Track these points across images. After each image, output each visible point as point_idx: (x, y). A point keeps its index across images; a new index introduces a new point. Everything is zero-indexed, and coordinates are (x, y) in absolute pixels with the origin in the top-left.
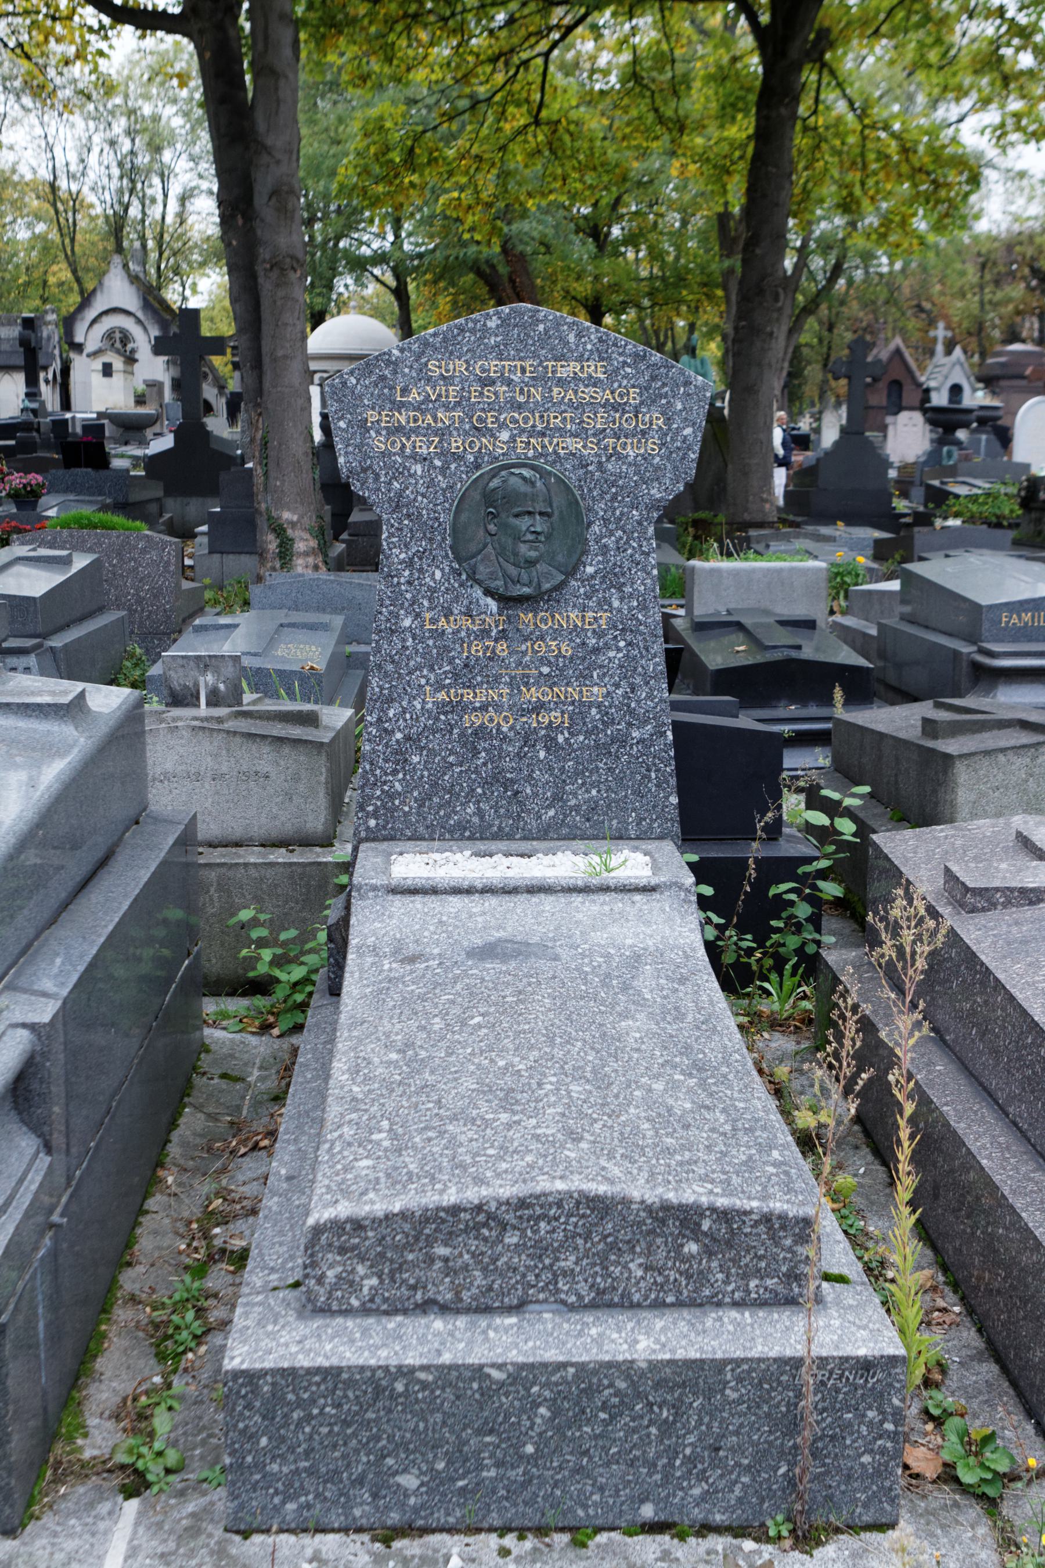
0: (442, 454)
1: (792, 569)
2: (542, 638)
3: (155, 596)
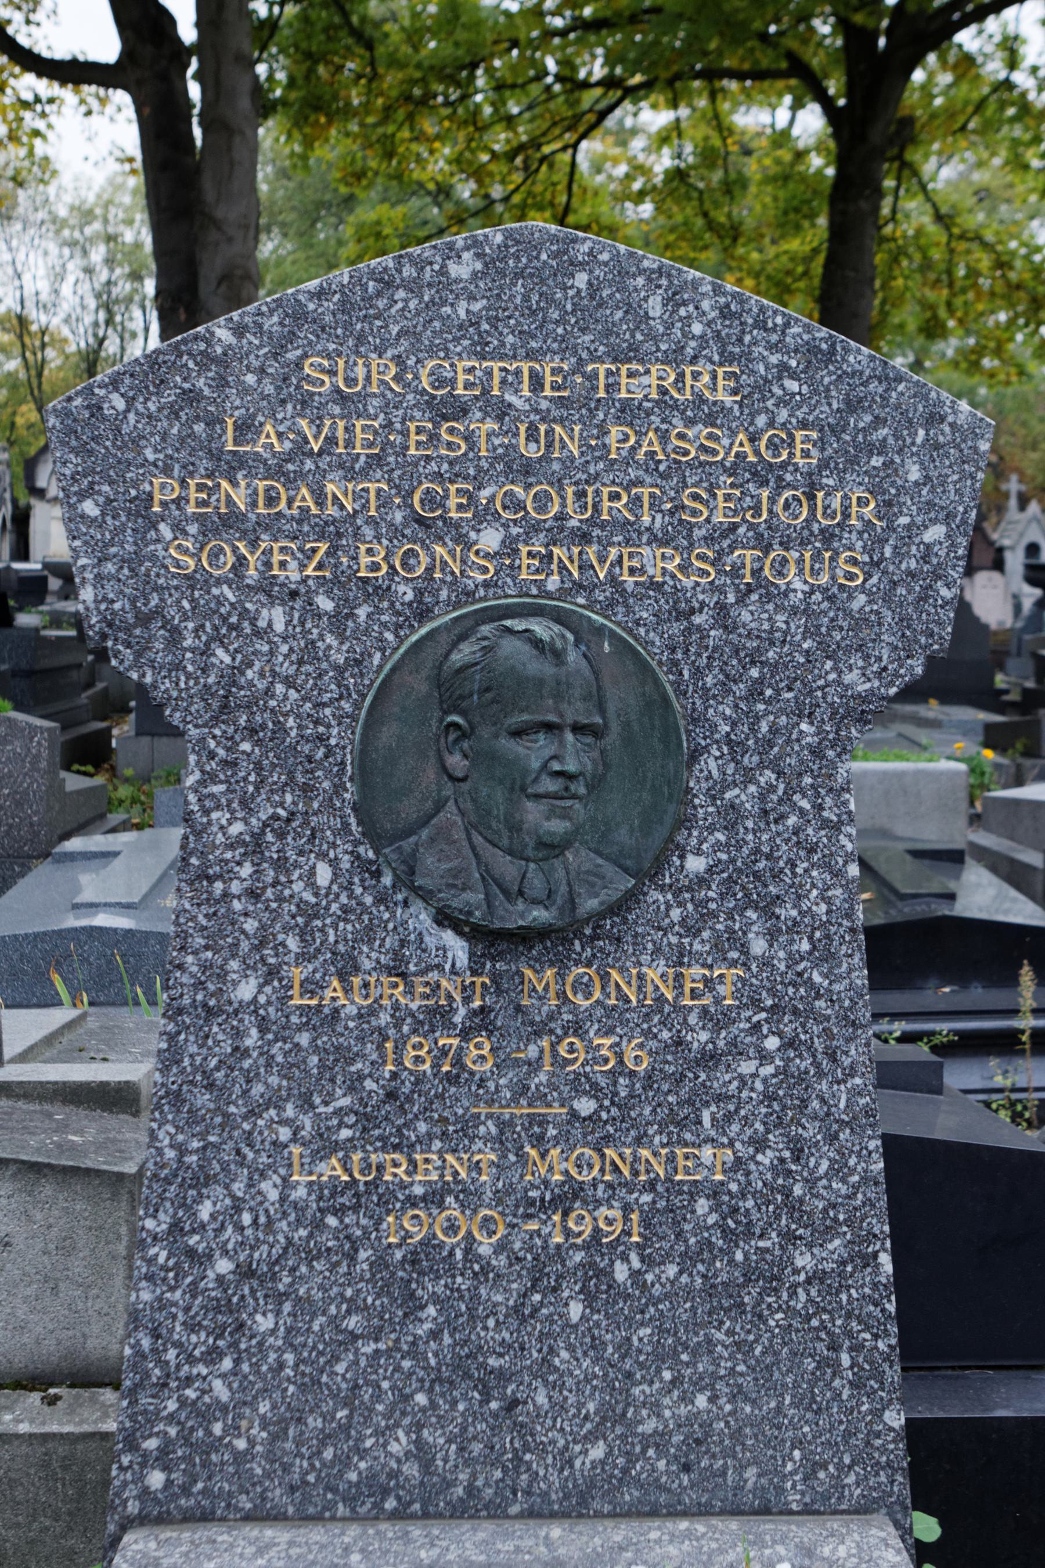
0: (337, 582)
1: (918, 773)
2: (577, 1028)
3: (19, 804)
